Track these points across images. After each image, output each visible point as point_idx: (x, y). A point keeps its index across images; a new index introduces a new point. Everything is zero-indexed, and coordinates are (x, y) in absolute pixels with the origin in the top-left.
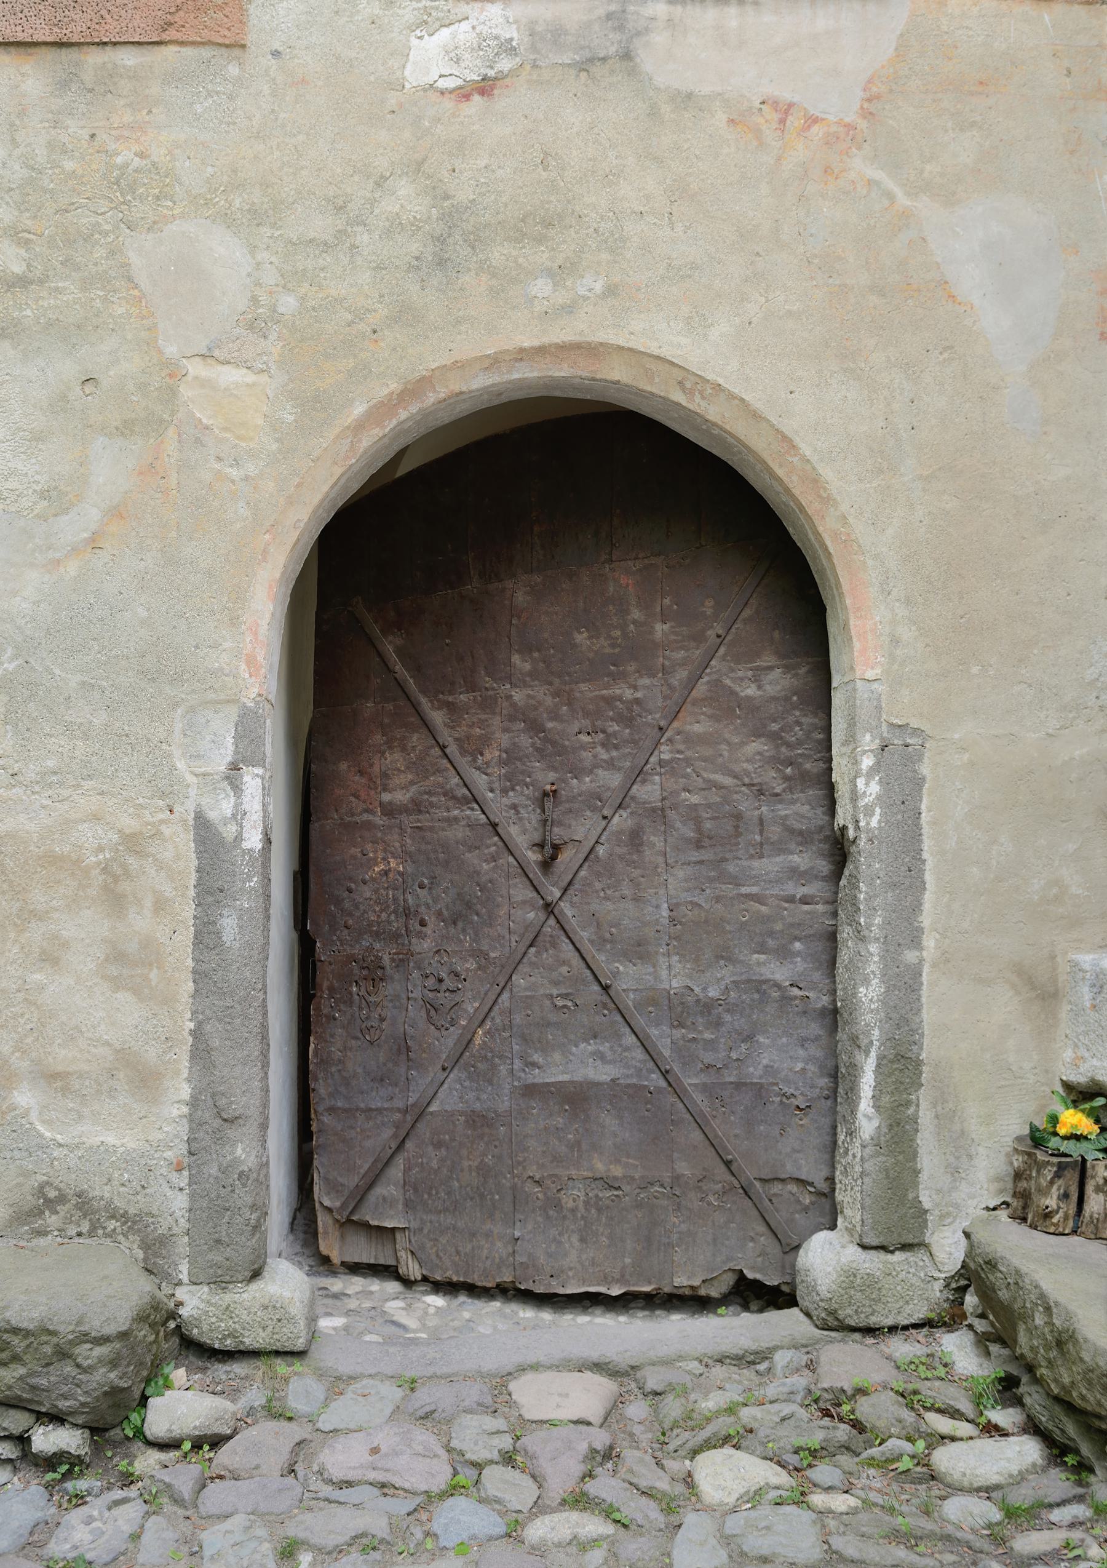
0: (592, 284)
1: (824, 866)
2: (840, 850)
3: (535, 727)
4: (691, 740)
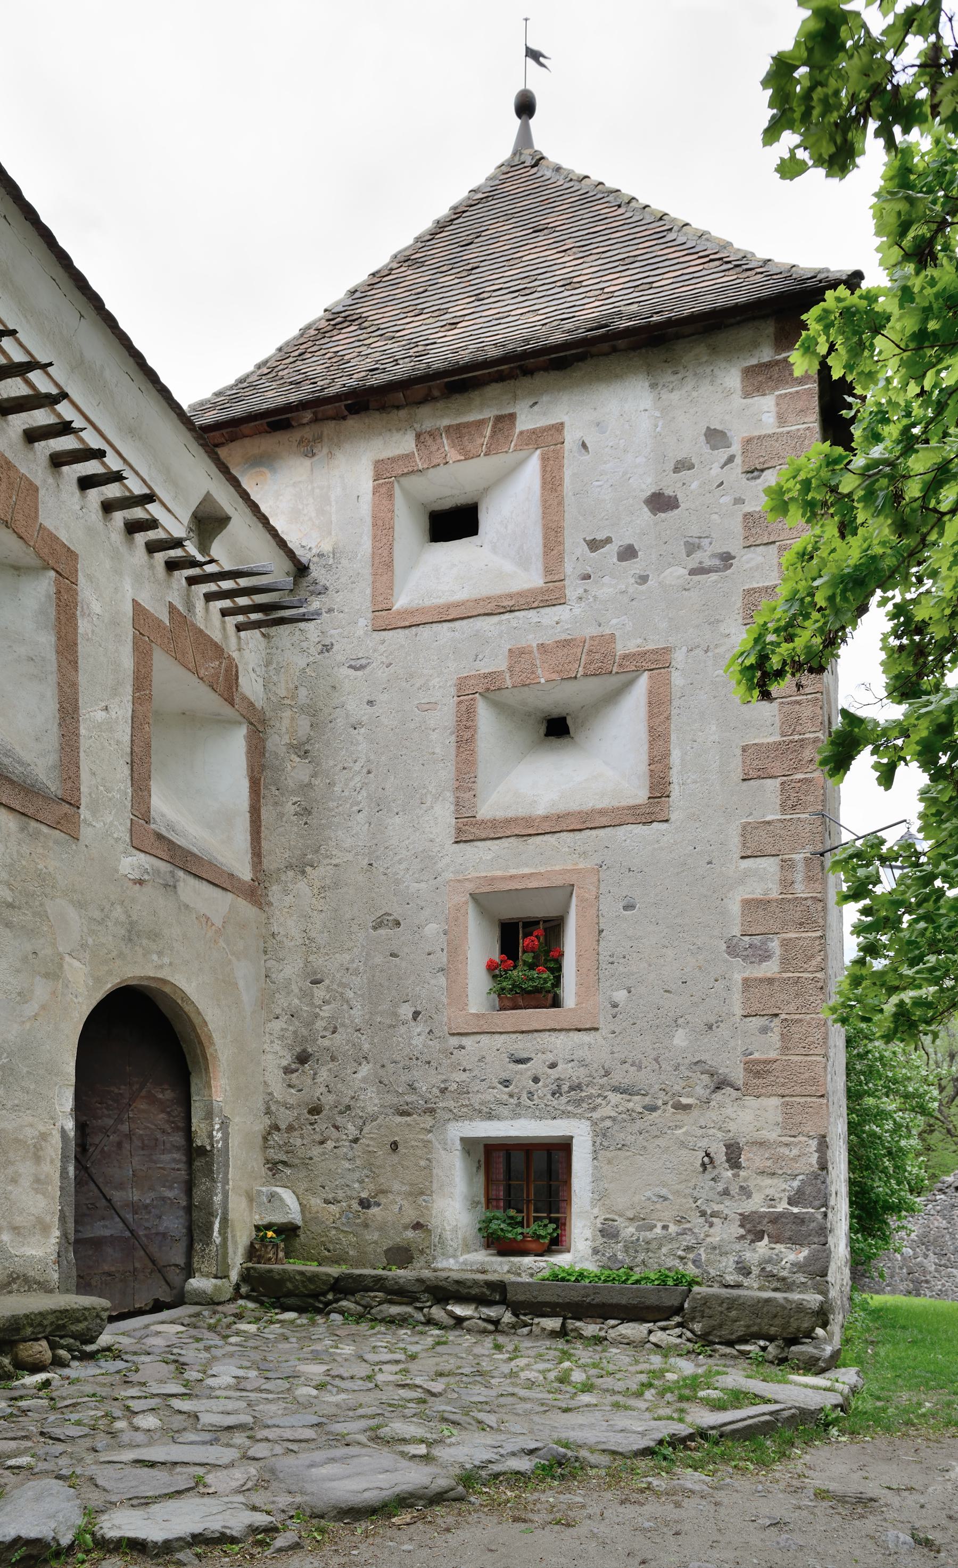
0: (166, 960)
1: (184, 1158)
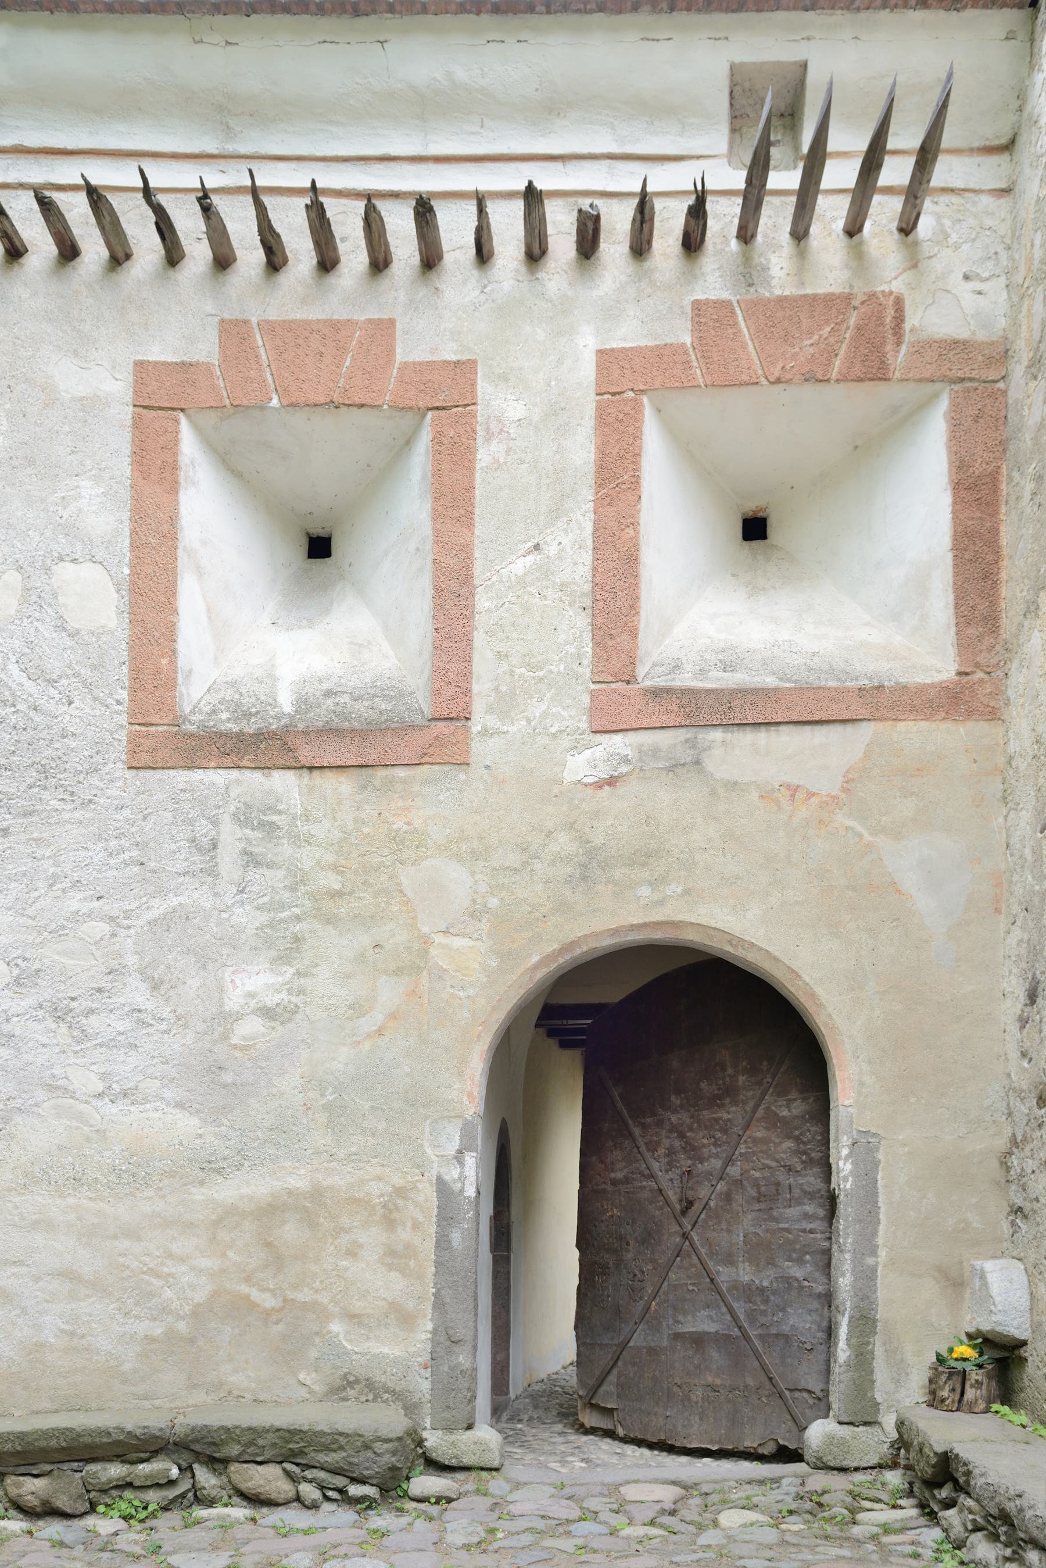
1: (821, 1212)
2: (832, 1201)
3: (682, 1136)
4: (755, 1141)
